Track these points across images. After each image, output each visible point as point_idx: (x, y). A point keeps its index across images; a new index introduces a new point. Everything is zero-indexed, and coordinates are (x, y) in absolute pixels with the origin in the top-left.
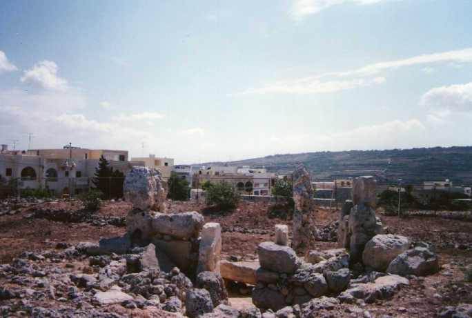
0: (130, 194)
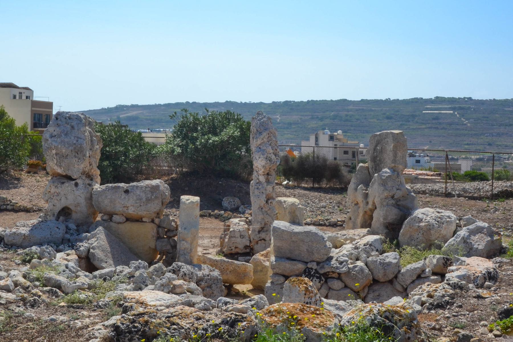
0: (57, 154)
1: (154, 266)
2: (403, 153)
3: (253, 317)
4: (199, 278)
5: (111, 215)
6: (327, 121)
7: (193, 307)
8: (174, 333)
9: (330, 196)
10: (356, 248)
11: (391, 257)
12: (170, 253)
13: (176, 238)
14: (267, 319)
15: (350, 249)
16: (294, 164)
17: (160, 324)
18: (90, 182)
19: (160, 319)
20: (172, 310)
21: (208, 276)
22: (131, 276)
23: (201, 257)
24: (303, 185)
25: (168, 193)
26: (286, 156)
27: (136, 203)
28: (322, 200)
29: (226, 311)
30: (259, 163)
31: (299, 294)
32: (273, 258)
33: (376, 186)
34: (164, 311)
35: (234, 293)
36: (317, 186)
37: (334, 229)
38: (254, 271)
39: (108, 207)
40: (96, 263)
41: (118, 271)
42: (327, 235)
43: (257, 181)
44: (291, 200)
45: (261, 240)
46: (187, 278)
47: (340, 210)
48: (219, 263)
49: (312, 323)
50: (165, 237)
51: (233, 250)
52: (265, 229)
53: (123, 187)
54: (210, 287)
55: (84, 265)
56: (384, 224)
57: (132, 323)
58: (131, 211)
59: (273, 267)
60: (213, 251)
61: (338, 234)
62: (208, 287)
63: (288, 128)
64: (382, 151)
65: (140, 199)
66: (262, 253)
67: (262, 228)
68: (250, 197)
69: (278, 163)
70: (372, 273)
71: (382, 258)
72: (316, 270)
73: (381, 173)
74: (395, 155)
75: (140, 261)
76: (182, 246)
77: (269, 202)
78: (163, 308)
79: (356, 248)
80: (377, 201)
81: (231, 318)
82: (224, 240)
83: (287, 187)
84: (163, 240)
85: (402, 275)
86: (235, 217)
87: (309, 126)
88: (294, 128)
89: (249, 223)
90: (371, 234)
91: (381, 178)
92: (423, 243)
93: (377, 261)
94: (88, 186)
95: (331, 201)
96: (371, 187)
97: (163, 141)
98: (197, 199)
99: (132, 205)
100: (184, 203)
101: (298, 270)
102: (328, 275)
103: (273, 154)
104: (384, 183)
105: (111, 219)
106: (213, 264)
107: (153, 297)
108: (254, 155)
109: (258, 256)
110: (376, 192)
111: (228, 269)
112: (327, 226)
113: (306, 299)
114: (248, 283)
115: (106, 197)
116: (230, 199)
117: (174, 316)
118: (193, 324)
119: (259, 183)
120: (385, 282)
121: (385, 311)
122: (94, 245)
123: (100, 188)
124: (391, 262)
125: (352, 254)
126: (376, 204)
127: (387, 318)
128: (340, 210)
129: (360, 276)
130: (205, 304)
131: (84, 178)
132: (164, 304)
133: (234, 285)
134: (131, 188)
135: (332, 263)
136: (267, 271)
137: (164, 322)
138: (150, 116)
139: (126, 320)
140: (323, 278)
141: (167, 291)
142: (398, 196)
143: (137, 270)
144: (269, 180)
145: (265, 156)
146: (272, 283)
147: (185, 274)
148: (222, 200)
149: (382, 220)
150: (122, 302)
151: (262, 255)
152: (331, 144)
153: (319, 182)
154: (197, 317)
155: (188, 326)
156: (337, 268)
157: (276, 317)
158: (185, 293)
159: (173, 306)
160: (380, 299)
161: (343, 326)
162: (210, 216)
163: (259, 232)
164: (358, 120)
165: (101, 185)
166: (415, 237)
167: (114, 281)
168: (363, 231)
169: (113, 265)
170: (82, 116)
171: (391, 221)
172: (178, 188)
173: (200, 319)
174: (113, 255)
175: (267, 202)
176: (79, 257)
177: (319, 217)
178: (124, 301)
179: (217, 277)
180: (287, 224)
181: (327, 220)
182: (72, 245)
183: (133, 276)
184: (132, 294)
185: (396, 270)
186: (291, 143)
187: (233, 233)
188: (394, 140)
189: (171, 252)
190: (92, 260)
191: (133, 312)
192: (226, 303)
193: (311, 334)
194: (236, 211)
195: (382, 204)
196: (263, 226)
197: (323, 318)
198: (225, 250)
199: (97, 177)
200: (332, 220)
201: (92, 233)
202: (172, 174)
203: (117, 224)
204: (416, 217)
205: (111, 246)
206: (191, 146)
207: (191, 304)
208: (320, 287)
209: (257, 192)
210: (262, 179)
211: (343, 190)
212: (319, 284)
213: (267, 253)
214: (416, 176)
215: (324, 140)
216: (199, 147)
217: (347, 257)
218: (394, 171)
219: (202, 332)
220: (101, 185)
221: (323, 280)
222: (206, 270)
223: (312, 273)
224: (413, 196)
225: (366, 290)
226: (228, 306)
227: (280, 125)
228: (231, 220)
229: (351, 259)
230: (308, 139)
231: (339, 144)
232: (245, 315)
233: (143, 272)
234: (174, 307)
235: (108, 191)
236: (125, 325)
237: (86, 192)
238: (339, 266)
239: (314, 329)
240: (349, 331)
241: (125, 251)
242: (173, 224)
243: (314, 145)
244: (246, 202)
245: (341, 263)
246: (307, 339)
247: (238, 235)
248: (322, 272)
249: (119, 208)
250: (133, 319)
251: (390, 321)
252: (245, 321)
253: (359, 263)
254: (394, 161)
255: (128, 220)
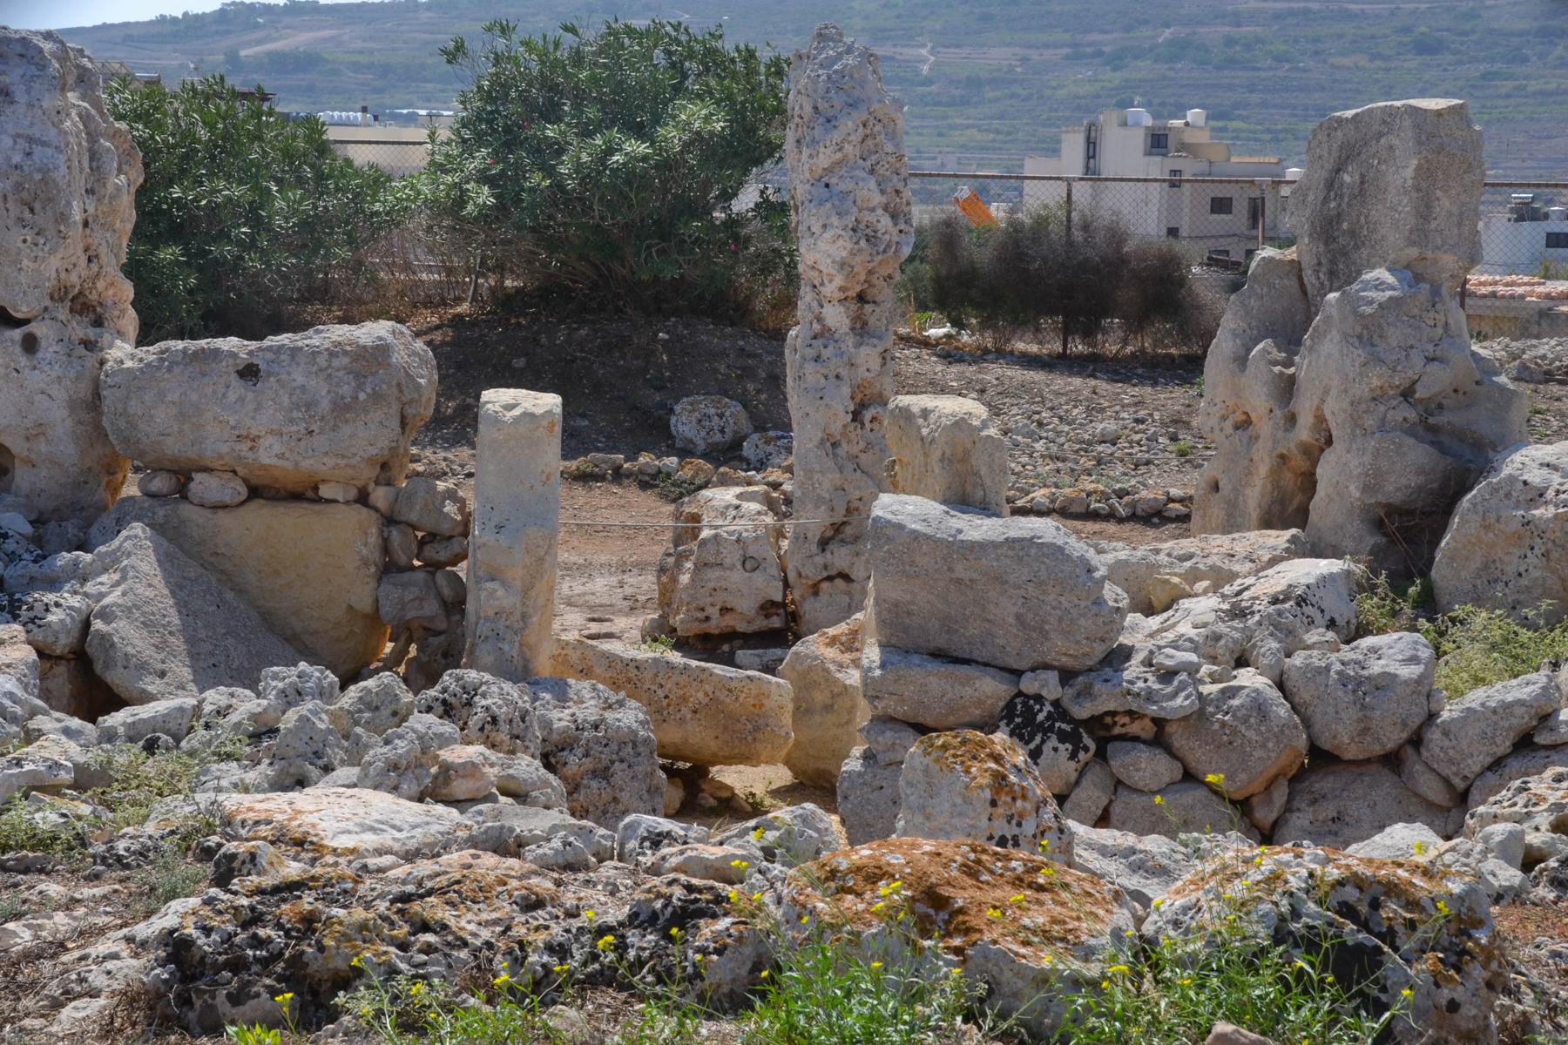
1: (362, 684)
2: (1463, 197)
3: (768, 898)
4: (555, 736)
5: (182, 475)
6: (1142, 69)
7: (518, 855)
8: (425, 964)
9: (1136, 391)
10: (1238, 613)
11: (1393, 652)
12: (438, 633)
13: (461, 570)
14: (820, 905)
15: (1211, 617)
16: (982, 256)
17: (363, 926)
18: (91, 333)
19: (368, 906)
20: (424, 867)
21: (596, 727)
22: (261, 732)
23: (569, 651)
24: (1020, 346)
25: (426, 378)
26: (948, 223)
27: (292, 421)
28: (1103, 410)
29: (654, 870)
30: (822, 252)
31: (967, 801)
32: (872, 654)
33: (1330, 346)
34: (391, 874)
35: (712, 802)
36: (1078, 347)
37: (1151, 533)
38: (797, 708)
39: (170, 441)
40: (116, 678)
41: (207, 708)
42: (1109, 558)
43: (817, 327)
44: (949, 406)
45: (830, 578)
46: (503, 736)
47: (1182, 454)
48: (648, 675)
49: (1009, 923)
50: (417, 563)
51: (713, 622)
52: (848, 530)
53: (234, 355)
54: (603, 773)
55: (67, 689)
56: (1366, 509)
57: (245, 925)
58: (271, 455)
59: (872, 690)
60: (630, 625)
61: (1157, 551)
62: (594, 774)
63: (965, 102)
64: (1361, 191)
65: (308, 406)
66: (831, 631)
67: (838, 528)
68: (786, 399)
69: (907, 251)
70: (1307, 723)
71: (1352, 656)
72: (1056, 703)
73: (1355, 287)
74: (1425, 211)
75: (303, 665)
76: (487, 601)
77: (868, 415)
78: (387, 860)
79: (1238, 613)
80: (1335, 411)
81: (669, 898)
82: (674, 580)
83: (950, 354)
84: (406, 576)
85: (1446, 734)
86: (724, 482)
87: (1062, 93)
88: (997, 100)
89: (780, 505)
90: (1304, 556)
91: (1355, 312)
92: (1547, 593)
93: (1328, 668)
94: (82, 350)
95: (1142, 414)
96: (1311, 349)
97: (418, 158)
98: (550, 402)
99: (272, 432)
100: (496, 420)
101: (980, 702)
102: (1108, 728)
103: (886, 209)
104: (1367, 333)
105: (182, 491)
106: (622, 678)
107: (348, 815)
108: (803, 215)
109: (813, 646)
110: (1330, 370)
111: (684, 699)
112: (1121, 521)
113: (996, 823)
114: (770, 761)
115: (161, 395)
116: (707, 406)
117: (430, 893)
118: (508, 928)
119: (824, 334)
120: (1368, 761)
121: (1341, 883)
122: (106, 601)
123: (132, 357)
124: (1396, 676)
125: (1217, 637)
126: (1332, 425)
127: (1347, 910)
128: (1182, 454)
129: (1251, 734)
130: (566, 844)
131: (63, 313)
132: (396, 846)
133: (714, 770)
134: (270, 356)
135: (1127, 675)
136: (851, 711)
137: (385, 919)
138: (371, 52)
139: (220, 913)
140: (1087, 740)
141: (415, 789)
142: (1437, 389)
143: (290, 704)
144: (865, 323)
145: (850, 221)
146: (868, 757)
147: (494, 720)
148: (672, 411)
149: (1354, 492)
150: (214, 840)
151: (833, 641)
152: (1157, 167)
153: (1088, 334)
154: (524, 898)
155: (486, 934)
156: (1150, 697)
157: (859, 895)
158: (489, 798)
159: (432, 850)
160: (1336, 832)
161: (1152, 942)
162: (618, 475)
163: (824, 544)
164: (1280, 59)
165: (140, 343)
166: (1511, 570)
167: (192, 754)
168: (1271, 542)
169: (192, 687)
170: (47, 46)
171: (1397, 498)
172: (471, 360)
173: (539, 904)
174: (192, 642)
175: (856, 416)
176: (40, 653)
177: (1087, 484)
178: (224, 835)
179: (635, 733)
180: (934, 509)
181: (1121, 494)
182: (11, 602)
183: (273, 732)
184: (258, 806)
185: (1414, 709)
186: (980, 166)
187: (711, 548)
188: (1420, 143)
189: (444, 626)
190: (98, 668)
191: (254, 880)
192: (656, 840)
193: (1008, 974)
194: (727, 455)
195: (1355, 422)
196: (838, 519)
197: (1063, 904)
198: (677, 620)
199: (123, 312)
200: (1144, 494)
201: (102, 549)
202: (458, 300)
203: (207, 513)
204: (1512, 479)
205: (182, 606)
206: (536, 179)
207: (507, 845)
208: (1074, 776)
209: (812, 373)
210: (837, 317)
211: (1188, 369)
212: (1073, 764)
213: (854, 633)
214: (1546, 304)
215: (1124, 151)
216: (570, 184)
217: (1195, 650)
218: (1418, 278)
219: (546, 958)
220: (140, 343)
221: (1086, 749)
222: (585, 704)
223: (1041, 717)
224: (1502, 389)
225: (1280, 795)
226: (665, 851)
227: (933, 88)
228: (707, 493)
229: (1213, 660)
230: (1054, 151)
231: (1189, 167)
232: (732, 892)
233: (315, 713)
234: (438, 855)
235: (169, 370)
236: (215, 937)
237: (72, 375)
238: (1156, 686)
239: (1023, 951)
240: (1181, 963)
241: (240, 625)
242: (450, 508)
243: (1077, 170)
244: (772, 420)
245: (1167, 675)
246: (990, 992)
247: (732, 556)
248: (1083, 711)
249: (216, 443)
250: (252, 909)
251: (1364, 926)
252: (726, 914)
253: (1250, 679)
254: (1419, 236)
255: (255, 492)
